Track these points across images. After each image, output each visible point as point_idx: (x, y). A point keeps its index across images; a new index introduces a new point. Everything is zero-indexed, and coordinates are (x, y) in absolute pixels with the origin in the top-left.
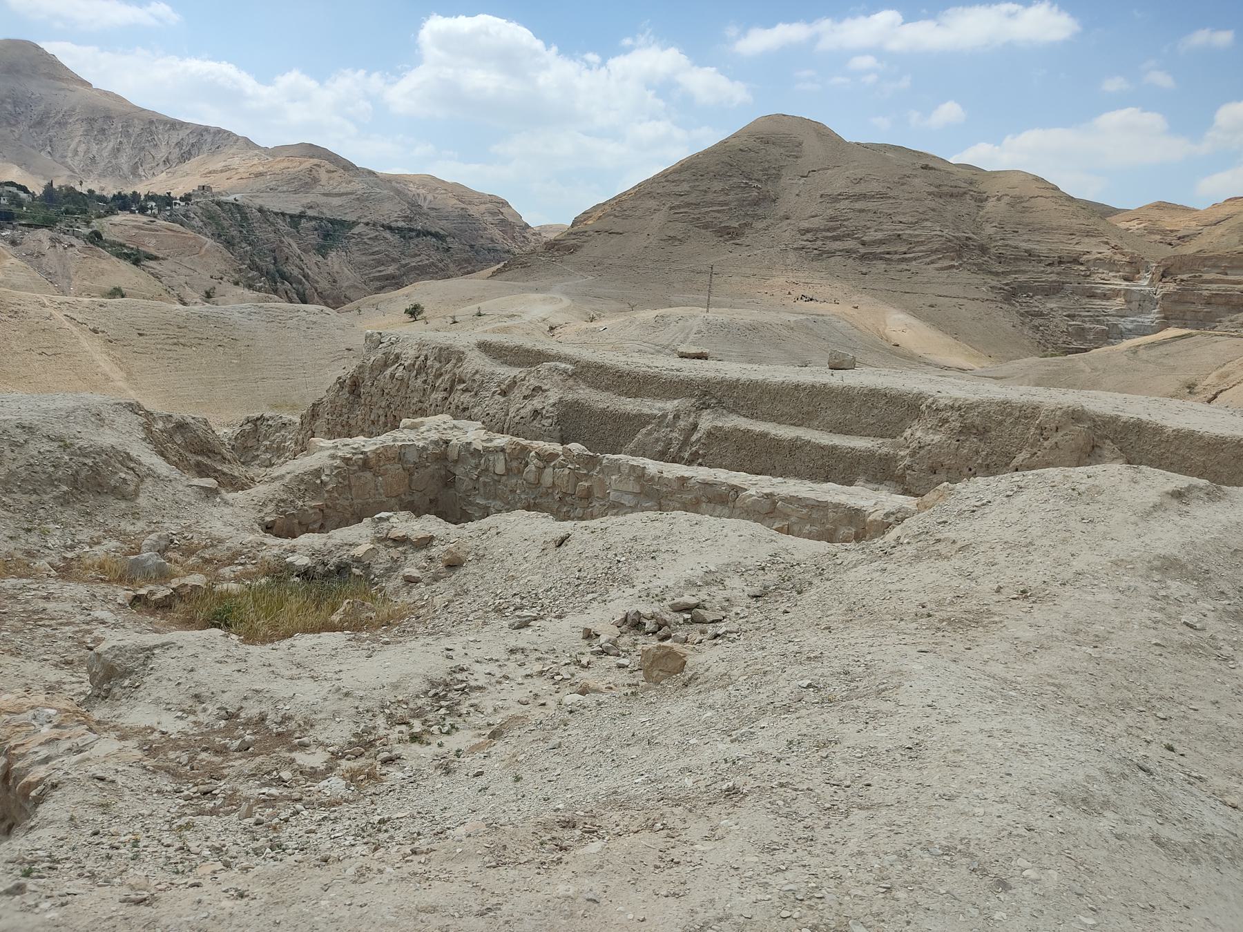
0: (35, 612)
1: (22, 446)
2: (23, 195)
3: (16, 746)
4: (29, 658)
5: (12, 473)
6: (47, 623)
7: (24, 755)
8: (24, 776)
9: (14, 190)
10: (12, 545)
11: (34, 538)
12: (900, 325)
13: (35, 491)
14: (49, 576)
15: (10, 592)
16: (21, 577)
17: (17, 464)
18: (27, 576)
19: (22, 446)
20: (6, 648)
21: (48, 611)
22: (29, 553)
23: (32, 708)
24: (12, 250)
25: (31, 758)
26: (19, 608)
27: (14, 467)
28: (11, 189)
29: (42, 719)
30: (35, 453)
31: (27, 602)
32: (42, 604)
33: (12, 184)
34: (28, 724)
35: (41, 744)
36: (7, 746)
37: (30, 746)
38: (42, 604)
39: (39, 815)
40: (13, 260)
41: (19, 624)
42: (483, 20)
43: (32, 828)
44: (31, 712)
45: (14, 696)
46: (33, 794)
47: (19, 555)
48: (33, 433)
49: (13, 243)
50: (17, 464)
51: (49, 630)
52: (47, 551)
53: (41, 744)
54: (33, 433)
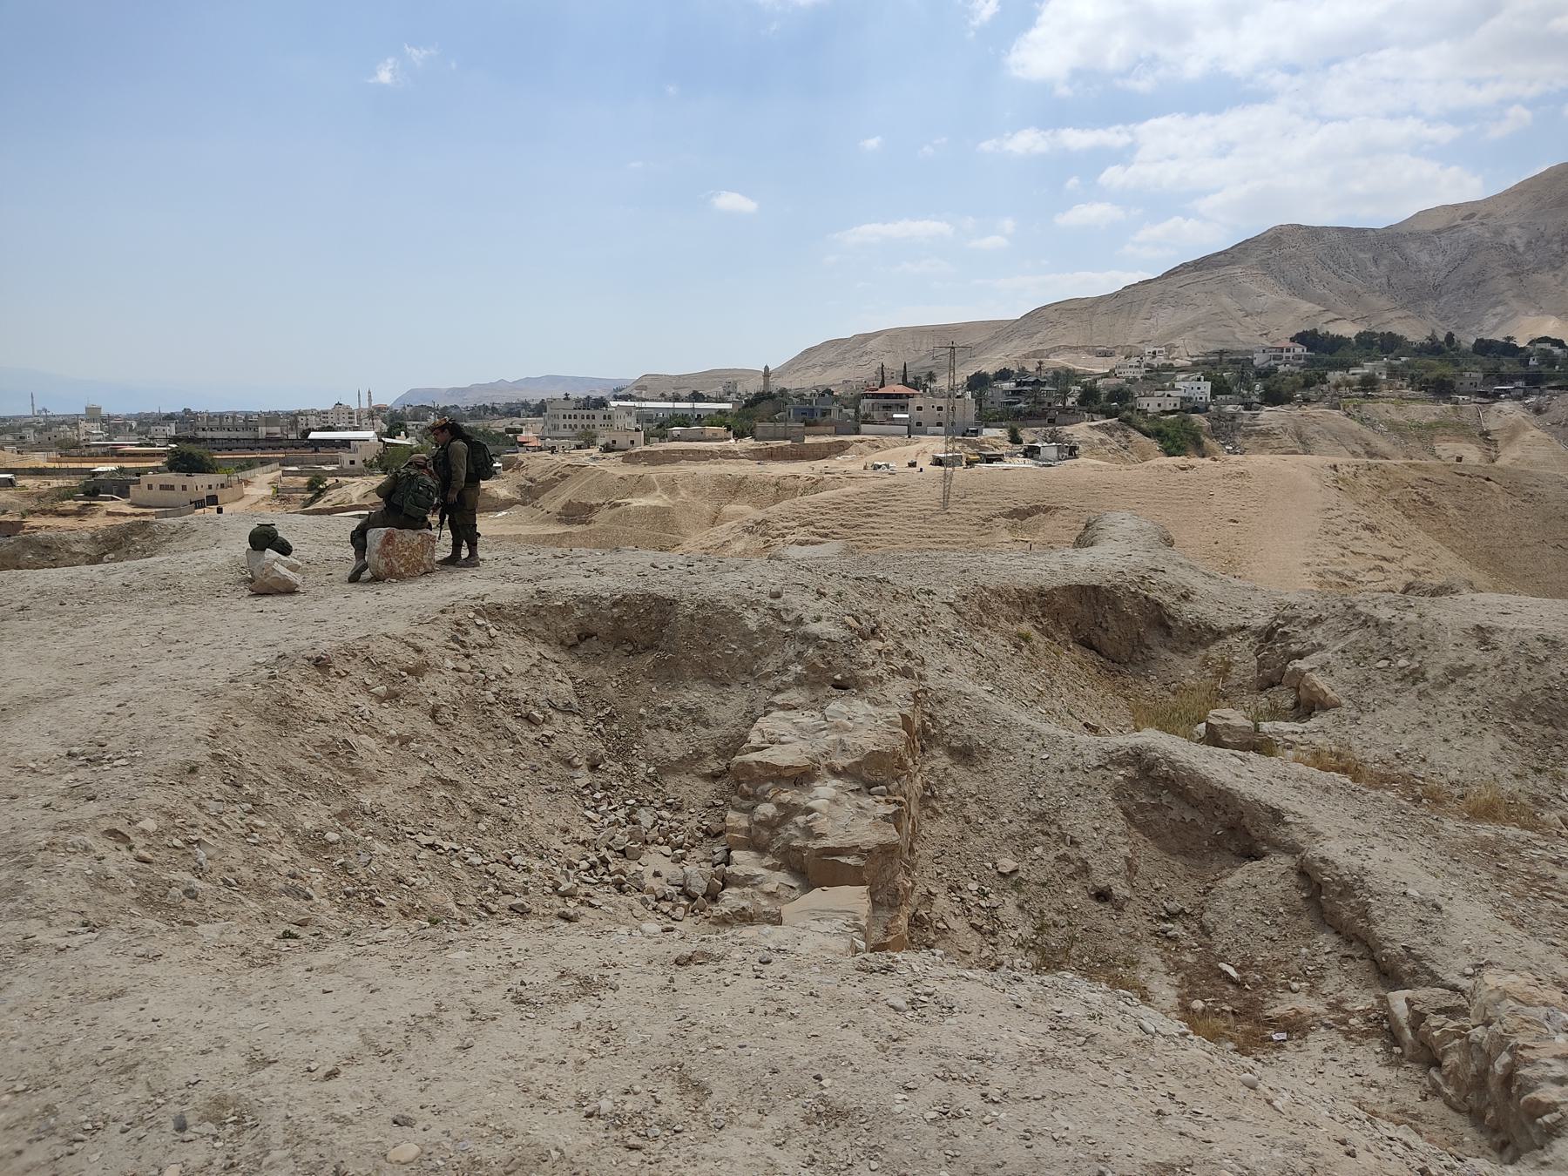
0: (1542, 877)
1: (1541, 663)
2: (1557, 351)
3: (1524, 1047)
4: (1534, 935)
5: (1525, 696)
6: (1557, 895)
7: (1533, 1062)
8: (1531, 1090)
9: (1547, 346)
10: (1517, 785)
11: (1544, 782)
12: (283, 570)
13: (1551, 723)
14: (1559, 834)
15: (1512, 843)
16: (1524, 827)
17: (1533, 685)
18: (1533, 829)
19: (1541, 663)
20: (1507, 913)
21: (1559, 881)
22: (1536, 799)
23: (1545, 1004)
24: (1535, 419)
25: (1542, 1070)
26: (1521, 866)
27: (1528, 689)
28: (1543, 346)
29: (1558, 1024)
30: (1558, 674)
31: (1532, 862)
32: (1551, 870)
33: (1546, 339)
34: (1540, 1025)
35: (1555, 1057)
36: (1513, 1042)
37: (1541, 1053)
38: (1551, 870)
39: (1556, 1151)
40: (1536, 432)
41: (1522, 888)
42: (868, 228)
43: (1545, 1163)
44: (1544, 1010)
45: (1522, 981)
46: (1547, 1118)
47: (1524, 799)
48: (1557, 649)
49: (1538, 411)
50: (1533, 685)
51: (1559, 906)
52: (1559, 802)
53: (1555, 1057)
54: (1557, 649)
